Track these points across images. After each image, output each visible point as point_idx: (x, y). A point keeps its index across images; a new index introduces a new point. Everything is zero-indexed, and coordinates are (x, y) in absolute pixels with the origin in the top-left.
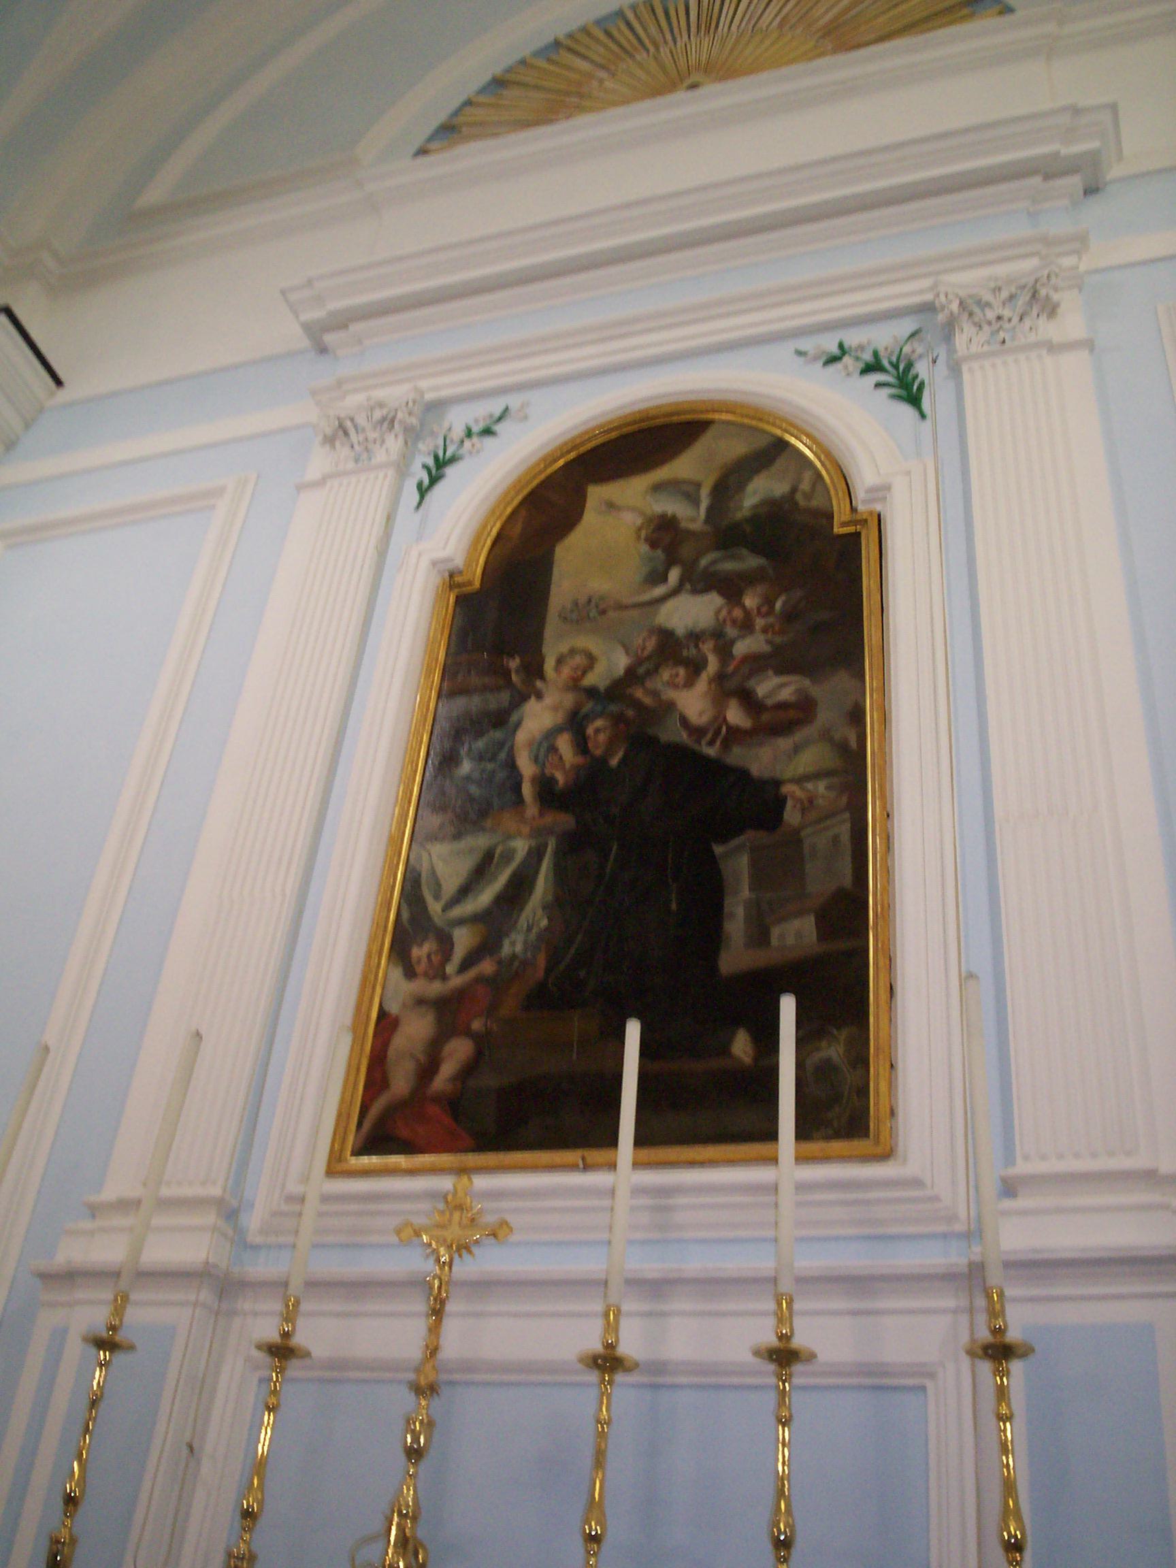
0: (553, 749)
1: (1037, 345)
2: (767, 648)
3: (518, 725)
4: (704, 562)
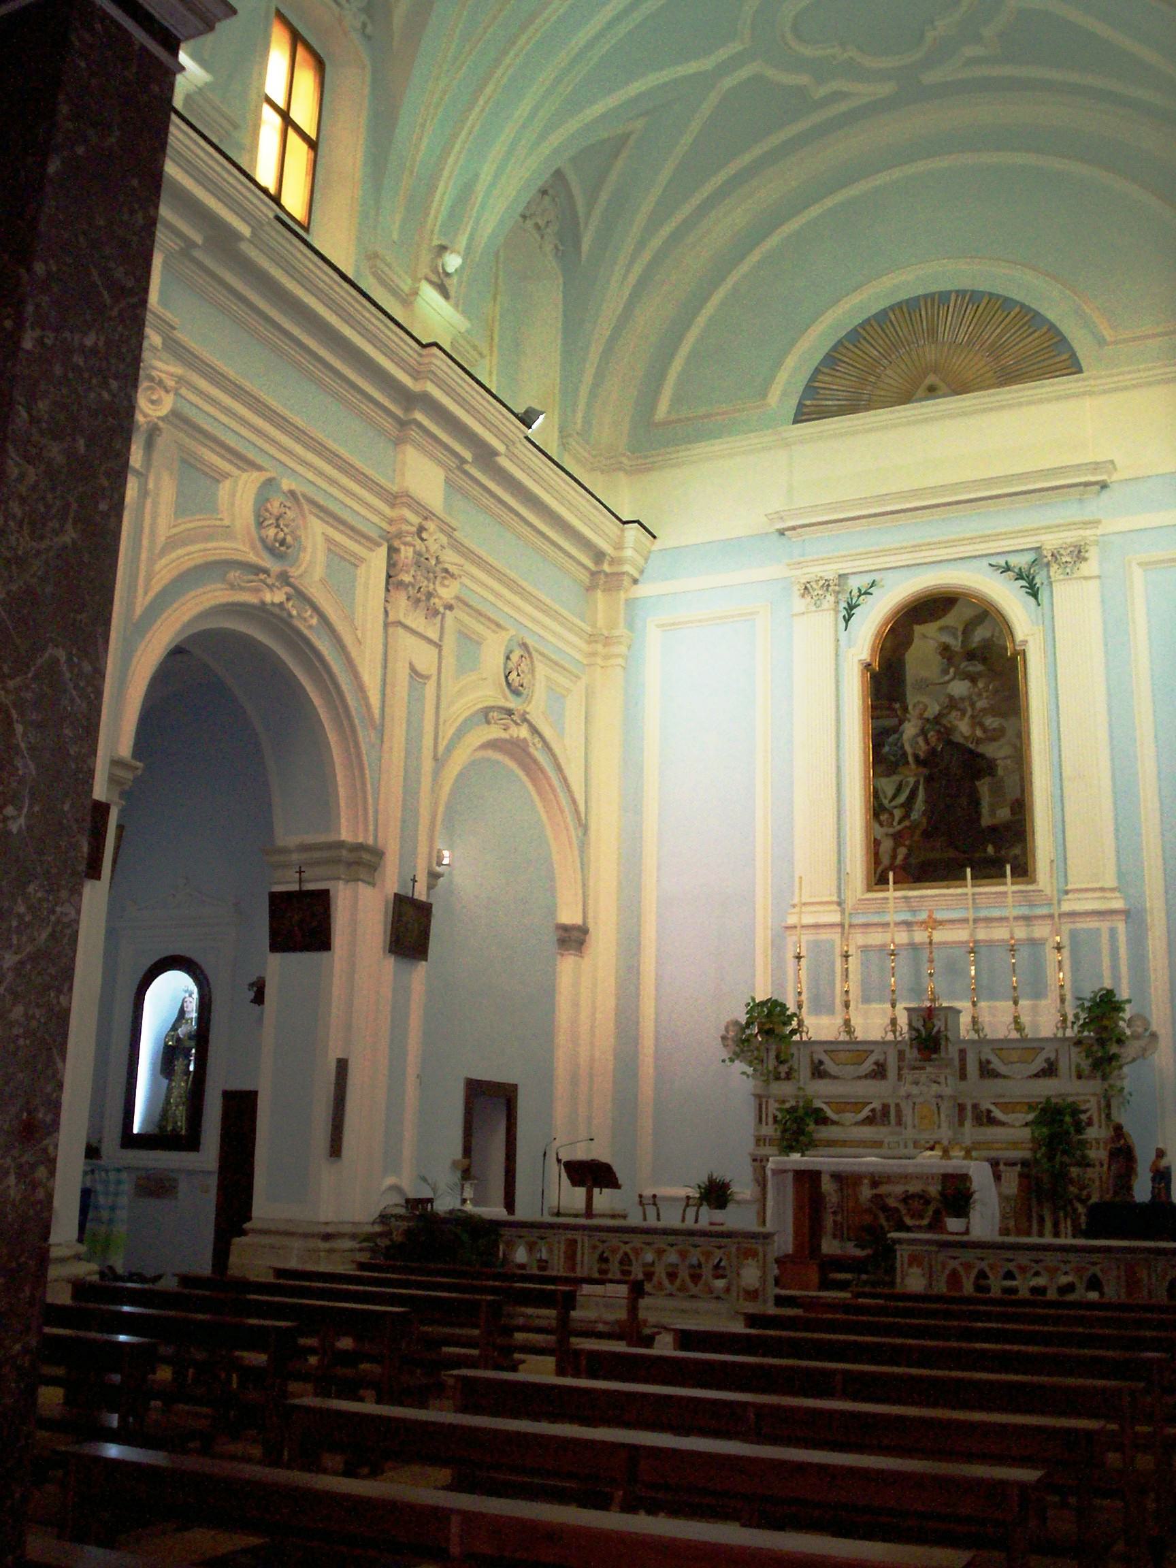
0: (917, 743)
2: (988, 706)
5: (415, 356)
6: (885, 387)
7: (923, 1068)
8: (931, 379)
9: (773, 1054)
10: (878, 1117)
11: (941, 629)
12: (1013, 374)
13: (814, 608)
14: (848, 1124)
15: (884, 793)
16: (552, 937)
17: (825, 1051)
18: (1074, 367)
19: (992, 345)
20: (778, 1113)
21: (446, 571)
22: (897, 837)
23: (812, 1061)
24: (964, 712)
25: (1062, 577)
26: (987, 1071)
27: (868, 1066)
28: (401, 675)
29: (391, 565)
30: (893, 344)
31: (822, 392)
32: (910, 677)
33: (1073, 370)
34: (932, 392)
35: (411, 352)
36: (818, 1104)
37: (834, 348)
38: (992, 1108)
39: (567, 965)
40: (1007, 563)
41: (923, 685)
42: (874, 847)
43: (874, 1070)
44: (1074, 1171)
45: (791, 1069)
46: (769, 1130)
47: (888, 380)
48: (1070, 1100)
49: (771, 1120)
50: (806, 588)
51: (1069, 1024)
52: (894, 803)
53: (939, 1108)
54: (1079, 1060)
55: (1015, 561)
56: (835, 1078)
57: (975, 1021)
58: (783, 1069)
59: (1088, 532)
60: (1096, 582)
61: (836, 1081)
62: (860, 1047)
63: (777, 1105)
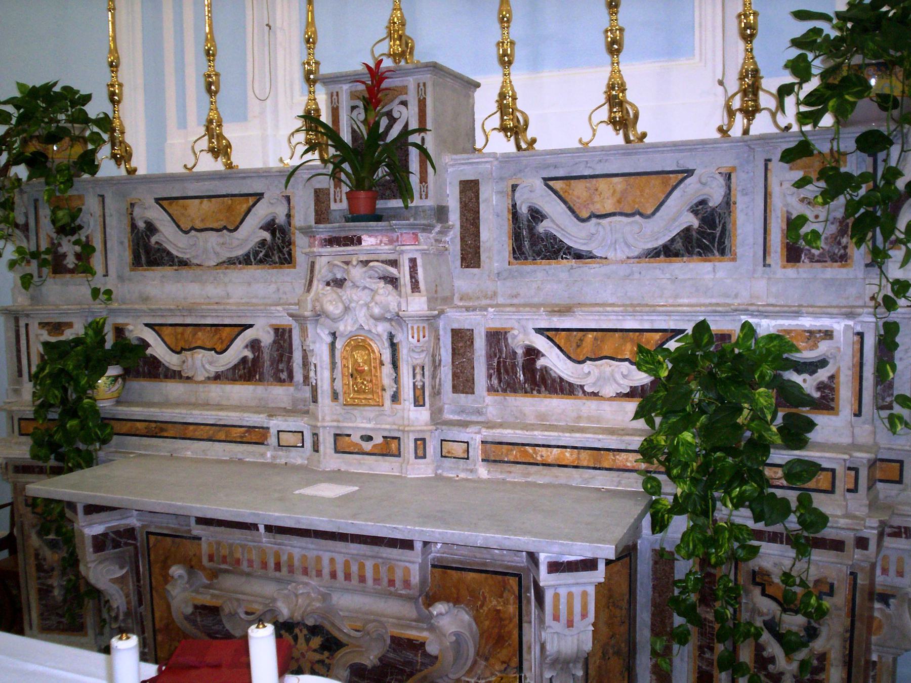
14: (201, 378)
23: (134, 226)
36: (138, 331)
38: (541, 343)
43: (263, 242)
51: (767, 101)
54: (798, 209)
56: (184, 263)
61: (184, 272)
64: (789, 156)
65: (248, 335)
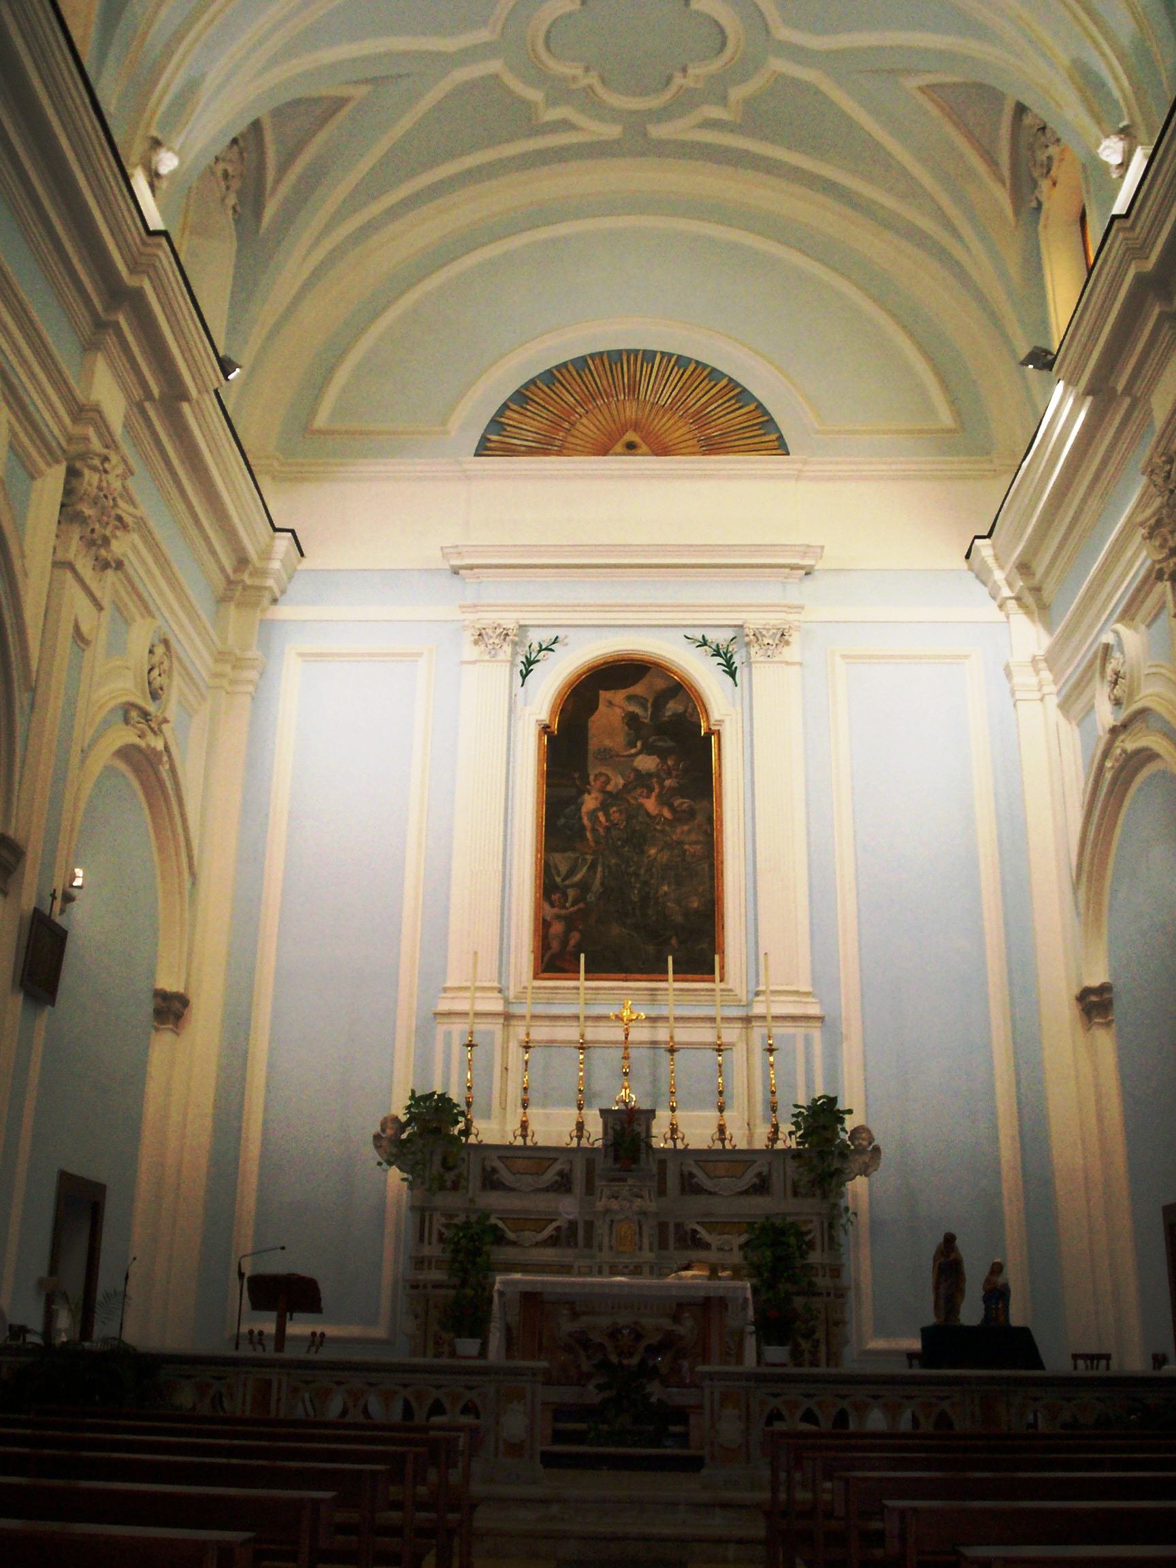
0: (597, 818)
1: (781, 662)
2: (676, 785)
3: (582, 804)
4: (651, 740)
5: (138, 241)
6: (579, 435)
7: (624, 1180)
8: (631, 436)
9: (437, 1159)
10: (565, 1237)
11: (630, 698)
12: (716, 446)
13: (487, 657)
15: (556, 867)
16: (149, 1007)
17: (499, 1158)
18: (781, 447)
19: (698, 412)
20: (443, 1230)
21: (119, 518)
22: (570, 923)
23: (484, 1169)
24: (651, 790)
25: (762, 659)
26: (690, 1186)
27: (550, 1176)
28: (66, 631)
29: (68, 492)
30: (591, 394)
31: (509, 429)
32: (594, 744)
33: (779, 451)
34: (631, 447)
35: (135, 234)
37: (526, 386)
38: (699, 1228)
39: (162, 1045)
40: (703, 637)
41: (606, 756)
42: (543, 928)
43: (556, 1182)
44: (799, 1302)
45: (459, 1176)
46: (432, 1250)
47: (582, 429)
48: (789, 1219)
49: (435, 1237)
50: (480, 635)
52: (567, 882)
53: (640, 1228)
55: (714, 636)
56: (511, 1189)
57: (674, 1129)
58: (450, 1177)
59: (791, 617)
60: (797, 667)
62: (538, 1154)
63: (443, 1220)
64: (793, 1157)
65: (555, 1225)
